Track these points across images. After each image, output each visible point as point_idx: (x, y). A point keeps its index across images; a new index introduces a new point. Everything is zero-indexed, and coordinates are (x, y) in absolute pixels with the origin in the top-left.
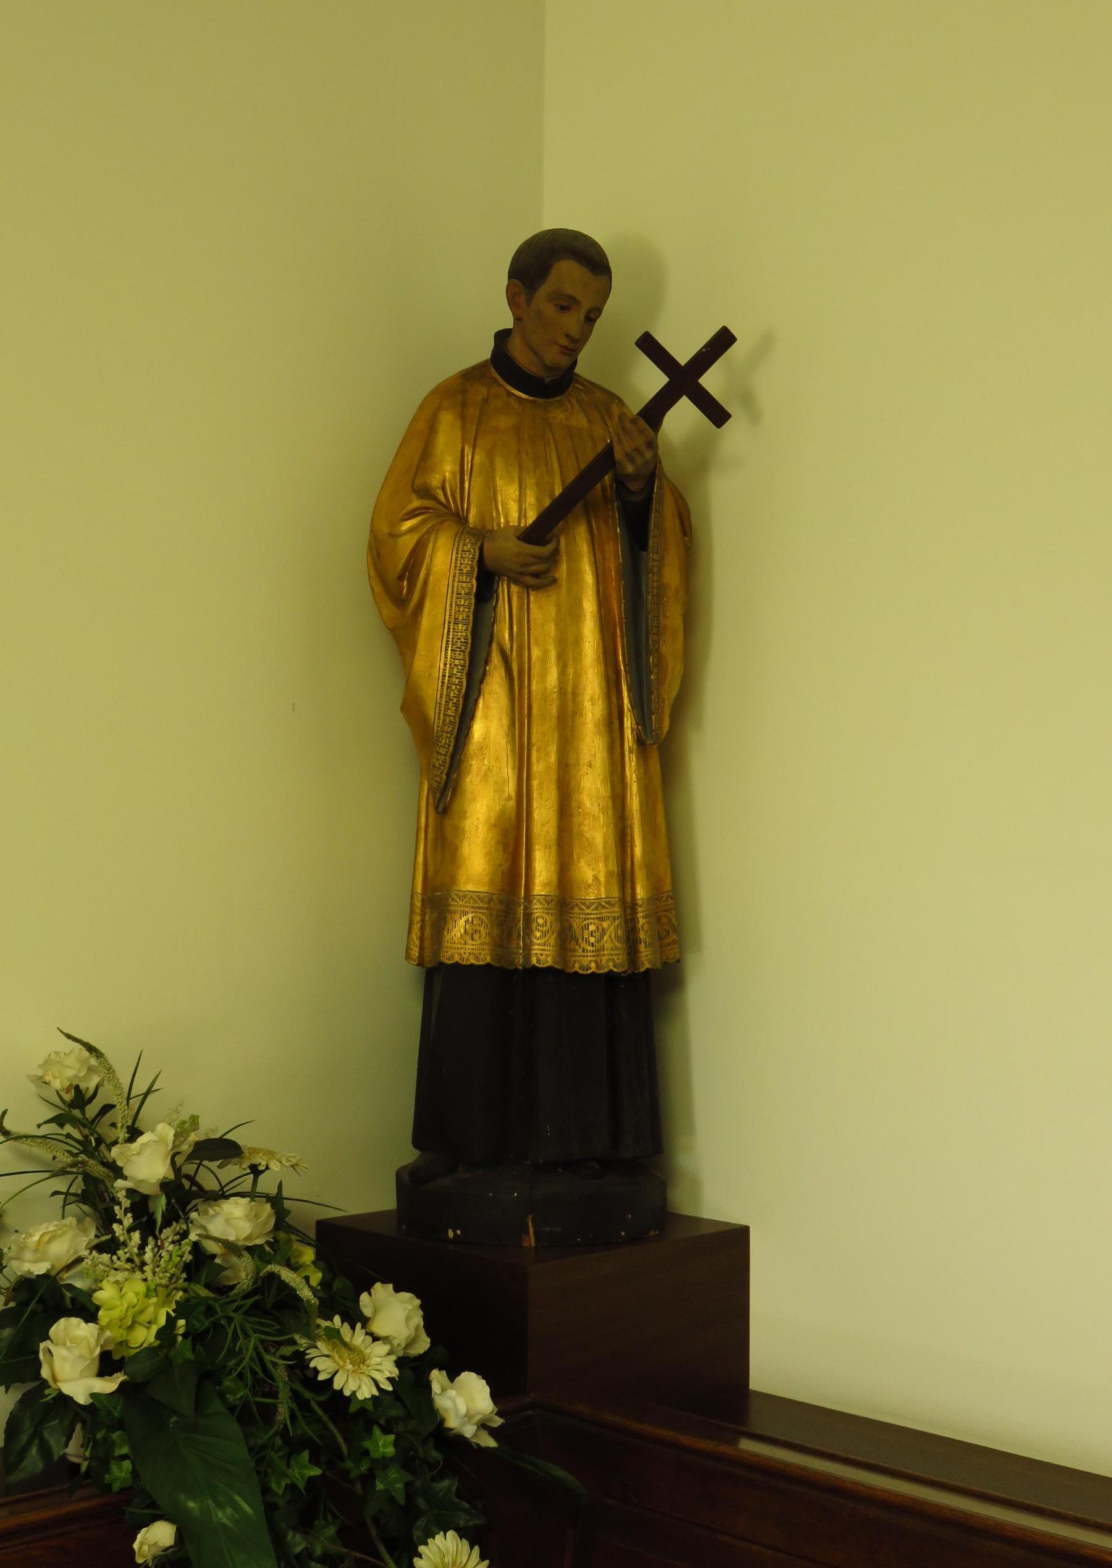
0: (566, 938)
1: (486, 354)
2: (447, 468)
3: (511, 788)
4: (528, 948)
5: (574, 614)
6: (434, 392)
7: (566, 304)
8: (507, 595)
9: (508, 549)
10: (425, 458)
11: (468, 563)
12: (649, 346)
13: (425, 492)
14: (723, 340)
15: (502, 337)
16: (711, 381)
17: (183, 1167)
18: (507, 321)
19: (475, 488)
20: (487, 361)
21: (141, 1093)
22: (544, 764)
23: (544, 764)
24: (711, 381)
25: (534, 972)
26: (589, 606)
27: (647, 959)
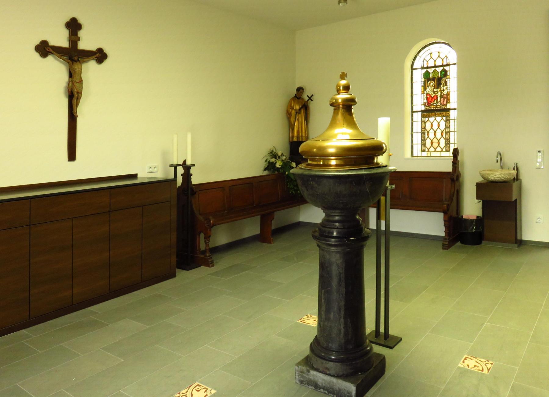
0: (302, 139)
1: (294, 96)
2: (293, 105)
3: (298, 128)
4: (299, 140)
5: (302, 116)
6: (291, 99)
7: (301, 92)
8: (297, 114)
9: (298, 111)
10: (291, 104)
11: (295, 112)
12: (308, 96)
13: (291, 107)
14: (313, 95)
15: (296, 94)
16: (310, 96)
17: (192, 167)
18: (296, 93)
19: (295, 106)
20: (473, 220)
21: (444, 146)
22: (300, 126)
23: (300, 126)
24: (310, 96)
25: (295, 142)
26: (303, 115)
27: (300, 140)
